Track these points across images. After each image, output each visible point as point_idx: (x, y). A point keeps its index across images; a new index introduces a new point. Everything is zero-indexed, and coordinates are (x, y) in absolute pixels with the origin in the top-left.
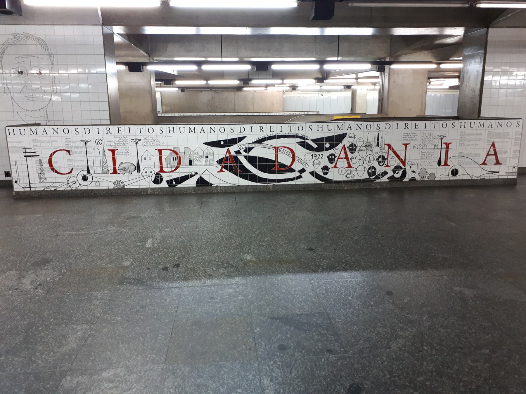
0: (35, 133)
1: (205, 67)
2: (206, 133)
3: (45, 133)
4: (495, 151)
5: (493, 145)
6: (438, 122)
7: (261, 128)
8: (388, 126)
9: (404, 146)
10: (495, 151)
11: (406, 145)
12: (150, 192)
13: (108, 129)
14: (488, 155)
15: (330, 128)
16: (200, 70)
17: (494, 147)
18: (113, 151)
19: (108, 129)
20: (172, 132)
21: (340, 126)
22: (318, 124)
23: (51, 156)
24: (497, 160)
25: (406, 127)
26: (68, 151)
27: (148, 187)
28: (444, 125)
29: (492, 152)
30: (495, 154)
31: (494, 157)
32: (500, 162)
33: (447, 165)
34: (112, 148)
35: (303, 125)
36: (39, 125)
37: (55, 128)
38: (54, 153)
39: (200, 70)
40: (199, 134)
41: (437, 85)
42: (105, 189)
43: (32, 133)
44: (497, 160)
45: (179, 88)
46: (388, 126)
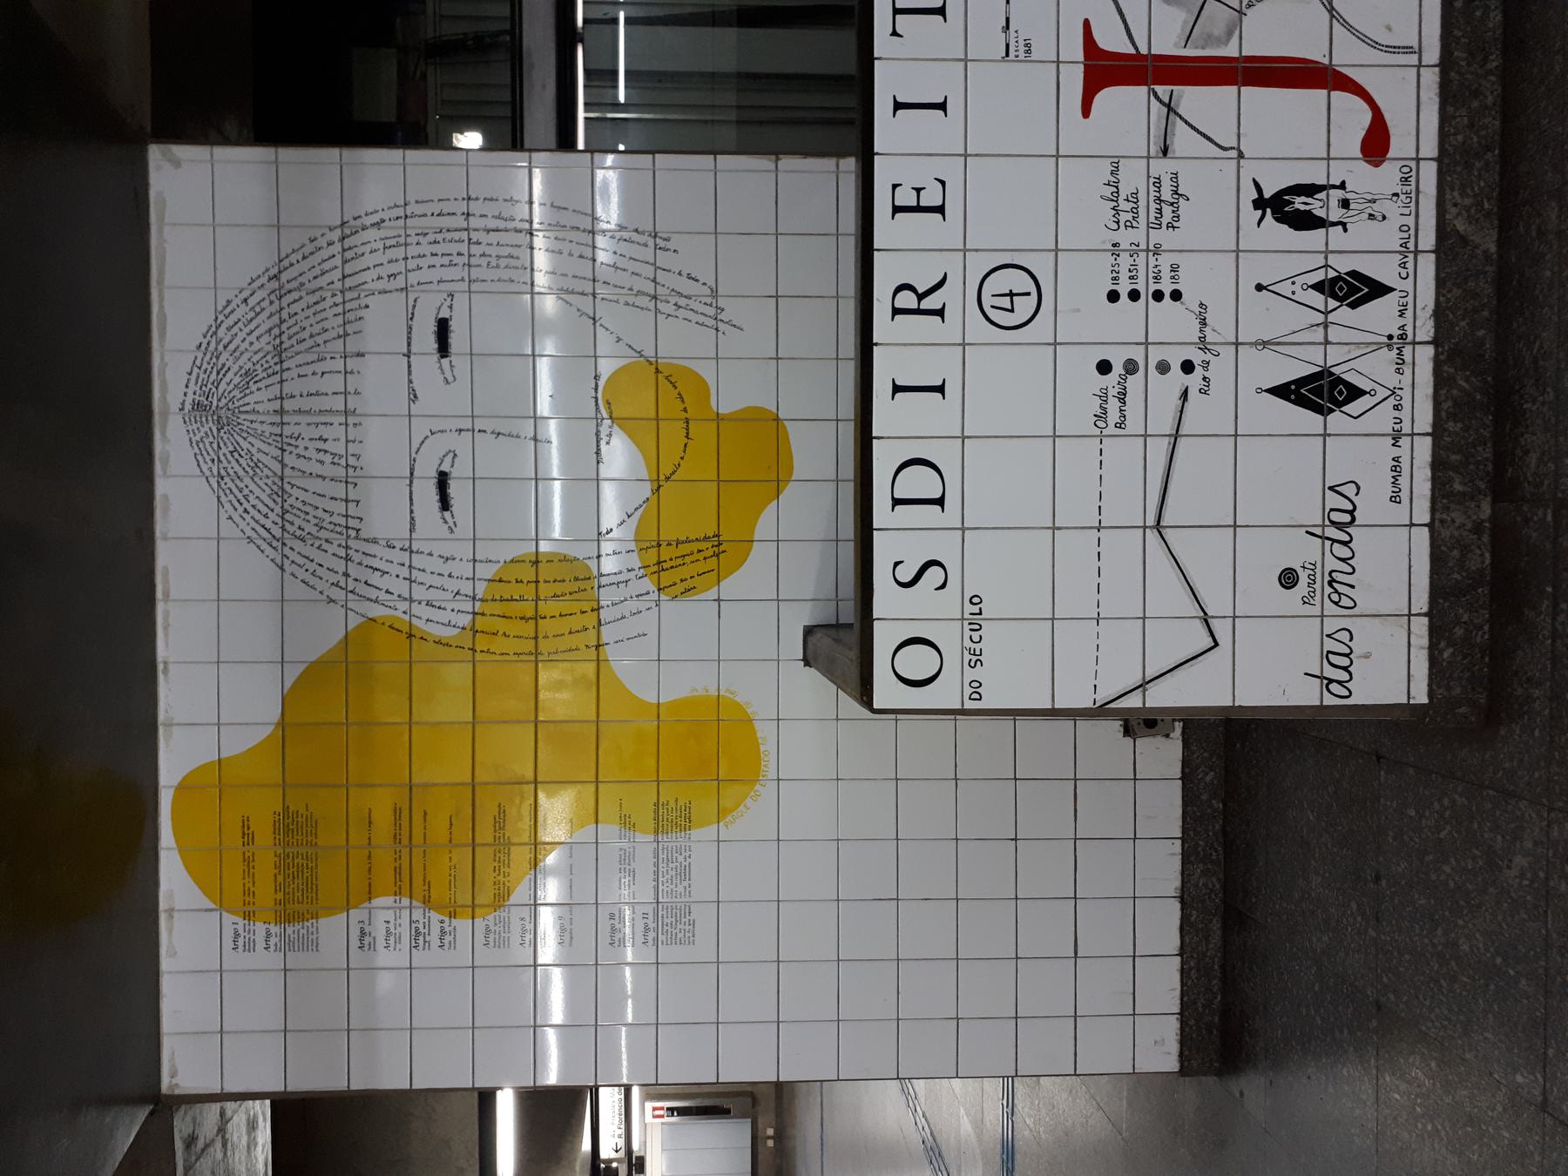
34: (1074, 79)
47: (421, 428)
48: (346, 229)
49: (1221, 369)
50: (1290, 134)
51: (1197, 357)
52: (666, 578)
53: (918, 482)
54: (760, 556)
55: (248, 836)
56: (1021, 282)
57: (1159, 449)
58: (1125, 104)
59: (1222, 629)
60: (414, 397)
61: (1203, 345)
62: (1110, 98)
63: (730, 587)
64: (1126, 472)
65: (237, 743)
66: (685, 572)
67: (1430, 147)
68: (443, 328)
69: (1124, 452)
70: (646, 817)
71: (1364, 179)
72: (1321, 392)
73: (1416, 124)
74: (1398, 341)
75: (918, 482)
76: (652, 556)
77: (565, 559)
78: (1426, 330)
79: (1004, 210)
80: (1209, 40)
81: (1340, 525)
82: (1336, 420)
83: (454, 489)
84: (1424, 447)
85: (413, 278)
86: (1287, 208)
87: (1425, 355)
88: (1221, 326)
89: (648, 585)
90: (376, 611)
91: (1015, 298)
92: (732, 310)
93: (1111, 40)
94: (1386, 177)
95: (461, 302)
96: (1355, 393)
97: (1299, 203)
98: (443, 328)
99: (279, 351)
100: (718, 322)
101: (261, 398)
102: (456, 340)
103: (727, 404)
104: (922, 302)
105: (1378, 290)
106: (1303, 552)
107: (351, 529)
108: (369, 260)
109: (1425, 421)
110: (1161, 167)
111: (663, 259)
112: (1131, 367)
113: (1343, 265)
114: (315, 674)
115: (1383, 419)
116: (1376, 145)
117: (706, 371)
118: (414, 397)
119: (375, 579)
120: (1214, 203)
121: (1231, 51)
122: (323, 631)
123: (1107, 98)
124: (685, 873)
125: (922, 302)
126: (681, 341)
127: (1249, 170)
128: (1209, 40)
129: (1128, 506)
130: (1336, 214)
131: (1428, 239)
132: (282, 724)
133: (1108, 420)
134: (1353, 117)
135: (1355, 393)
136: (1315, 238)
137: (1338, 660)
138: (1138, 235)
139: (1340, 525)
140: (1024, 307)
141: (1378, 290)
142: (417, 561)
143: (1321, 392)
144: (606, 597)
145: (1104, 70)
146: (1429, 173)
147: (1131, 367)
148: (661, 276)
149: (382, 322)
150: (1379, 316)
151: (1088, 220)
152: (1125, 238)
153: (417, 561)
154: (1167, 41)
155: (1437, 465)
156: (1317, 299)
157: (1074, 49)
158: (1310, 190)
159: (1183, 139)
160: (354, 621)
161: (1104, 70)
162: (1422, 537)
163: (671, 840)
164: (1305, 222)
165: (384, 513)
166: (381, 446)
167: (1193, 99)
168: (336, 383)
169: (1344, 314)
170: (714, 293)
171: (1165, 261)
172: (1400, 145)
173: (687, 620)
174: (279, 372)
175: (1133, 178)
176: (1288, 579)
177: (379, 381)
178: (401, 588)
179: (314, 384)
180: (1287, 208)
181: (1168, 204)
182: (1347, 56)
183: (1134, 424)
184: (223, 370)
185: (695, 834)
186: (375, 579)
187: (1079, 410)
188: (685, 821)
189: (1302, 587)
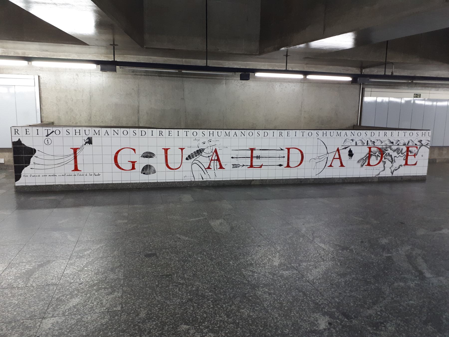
0: (98, 134)
1: (310, 77)
6: (189, 130)
7: (161, 132)
8: (266, 134)
11: (182, 149)
12: (258, 183)
14: (334, 158)
16: (305, 79)
17: (339, 152)
18: (166, 150)
19: (161, 132)
21: (227, 133)
22: (75, 128)
23: (117, 153)
24: (341, 163)
25: (281, 134)
26: (134, 150)
28: (251, 134)
29: (337, 156)
30: (218, 160)
32: (223, 166)
35: (197, 131)
37: (243, 131)
38: (117, 153)
39: (305, 79)
40: (113, 136)
41: (429, 100)
43: (95, 134)
44: (341, 163)
46: (266, 134)
53: (143, 133)
75: (143, 133)
157: (183, 147)
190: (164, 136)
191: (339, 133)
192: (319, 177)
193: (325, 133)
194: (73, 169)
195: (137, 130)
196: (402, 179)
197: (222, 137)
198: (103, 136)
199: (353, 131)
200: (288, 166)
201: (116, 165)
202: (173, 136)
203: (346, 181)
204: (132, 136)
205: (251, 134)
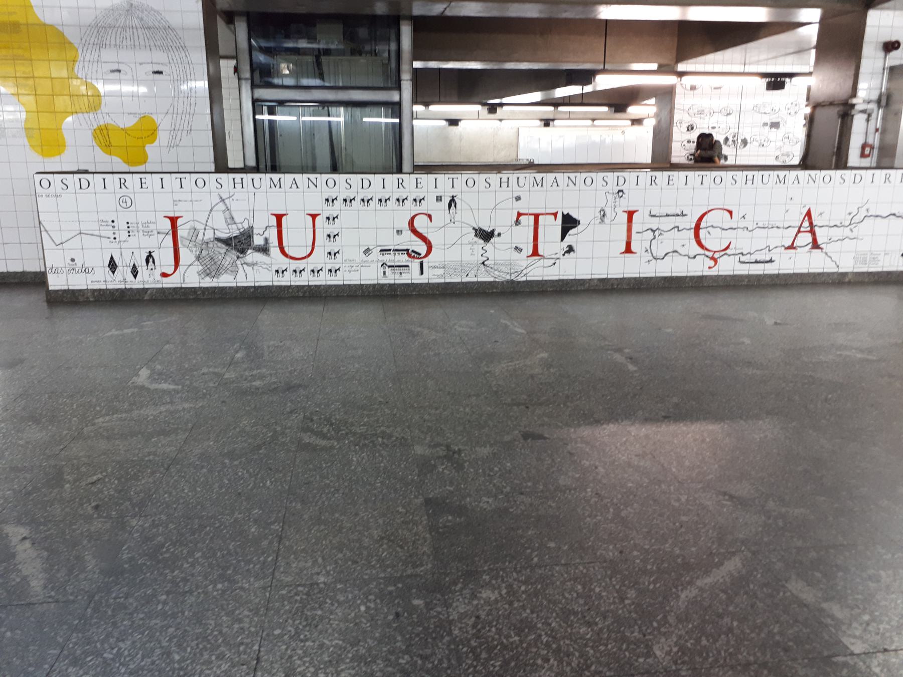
2: (561, 188)
3: (294, 186)
4: (811, 224)
5: (809, 214)
6: (708, 173)
9: (310, 218)
10: (811, 224)
13: (123, 181)
14: (799, 231)
15: (521, 183)
20: (238, 186)
26: (731, 213)
27: (197, 285)
30: (812, 232)
31: (809, 235)
33: (538, 255)
34: (171, 215)
36: (86, 172)
40: (549, 188)
42: (303, 286)
45: (447, 120)
47: (133, 66)
48: (184, 48)
49: (115, 245)
50: (165, 258)
51: (117, 240)
52: (98, 132)
53: (84, 184)
54: (107, 158)
55: (10, 14)
56: (129, 203)
57: (97, 233)
58: (168, 224)
59: (60, 246)
60: (141, 64)
61: (120, 242)
62: (168, 222)
63: (97, 149)
64: (93, 227)
65: (38, 12)
66: (100, 136)
67: (165, 286)
68: (160, 73)
69: (96, 226)
70: (29, 126)
71: (157, 273)
72: (113, 266)
73: (168, 283)
74: (125, 281)
75: (84, 184)
76: (103, 127)
77: (100, 104)
78: (128, 287)
79: (142, 200)
80: (182, 242)
81: (85, 271)
82: (108, 269)
83: (117, 74)
84: (104, 287)
85: (173, 65)
86: (149, 258)
87: (123, 287)
88: (124, 245)
89: (95, 127)
90: (80, 52)
91: (126, 203)
92: (173, 150)
93: (179, 222)
94: (158, 277)
95: (168, 78)
96: (113, 272)
97: (151, 260)
98: (160, 73)
99: (149, 28)
100: (170, 147)
101: (136, 22)
102: (157, 76)
103: (149, 149)
104: (122, 184)
105: (135, 276)
106: (79, 263)
107: (101, 46)
108: (176, 54)
109: (109, 287)
110: (155, 232)
111: (185, 133)
112: (114, 227)
113: (139, 269)
114: (61, 34)
115: (109, 278)
116: (164, 275)
117: (156, 143)
118: (141, 64)
119: (89, 52)
120: (150, 243)
121: (180, 245)
122: (71, 35)
123: (168, 221)
124: (14, 136)
125: (122, 184)
126: (163, 137)
127: (156, 251)
128: (182, 242)
129: (84, 228)
130: (150, 268)
131: (147, 286)
132: (45, 25)
133: (102, 222)
134: (169, 271)
135: (113, 272)
136: (144, 263)
137: (56, 271)
138: (140, 227)
139: (85, 271)
140: (124, 205)
141: (135, 276)
142: (95, 64)
143: (113, 266)
144: (91, 115)
145: (173, 220)
146: (160, 286)
147: (114, 227)
148: (180, 132)
149: (160, 57)
150: (130, 277)
151: (143, 218)
152: (140, 225)
153: (95, 64)
154: (180, 233)
155: (100, 290)
156: (132, 265)
157: (177, 215)
158: (154, 262)
159: (161, 237)
160: (76, 46)
161: (173, 220)
162: (85, 287)
163: (23, 132)
164: (147, 261)
165: (108, 55)
166: (126, 55)
167: (170, 238)
168: (142, 43)
169: (129, 270)
170: (177, 146)
171: (136, 233)
172: (165, 280)
173: (88, 138)
174: (143, 27)
175: (152, 227)
176: (73, 260)
177: (144, 55)
178: (87, 59)
179: (141, 37)
180: (149, 258)
181: (148, 234)
182: (181, 269)
183: (102, 228)
184: (142, 12)
185: (26, 139)
186: (89, 52)
187: (102, 217)
188: (29, 137)
189: (71, 263)
190: (659, 186)
191: (781, 177)
192: (221, 285)
193: (238, 180)
194: (623, 249)
195: (739, 173)
196: (749, 281)
197: (526, 187)
198: (287, 189)
199: (312, 176)
200: (535, 253)
201: (430, 242)
202: (675, 186)
203: (359, 293)
204: (482, 188)
205: (331, 183)
